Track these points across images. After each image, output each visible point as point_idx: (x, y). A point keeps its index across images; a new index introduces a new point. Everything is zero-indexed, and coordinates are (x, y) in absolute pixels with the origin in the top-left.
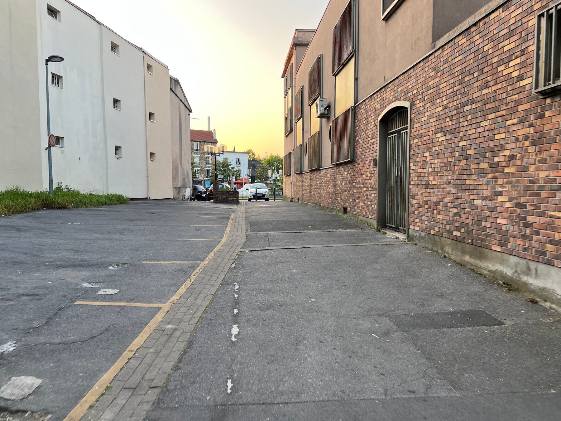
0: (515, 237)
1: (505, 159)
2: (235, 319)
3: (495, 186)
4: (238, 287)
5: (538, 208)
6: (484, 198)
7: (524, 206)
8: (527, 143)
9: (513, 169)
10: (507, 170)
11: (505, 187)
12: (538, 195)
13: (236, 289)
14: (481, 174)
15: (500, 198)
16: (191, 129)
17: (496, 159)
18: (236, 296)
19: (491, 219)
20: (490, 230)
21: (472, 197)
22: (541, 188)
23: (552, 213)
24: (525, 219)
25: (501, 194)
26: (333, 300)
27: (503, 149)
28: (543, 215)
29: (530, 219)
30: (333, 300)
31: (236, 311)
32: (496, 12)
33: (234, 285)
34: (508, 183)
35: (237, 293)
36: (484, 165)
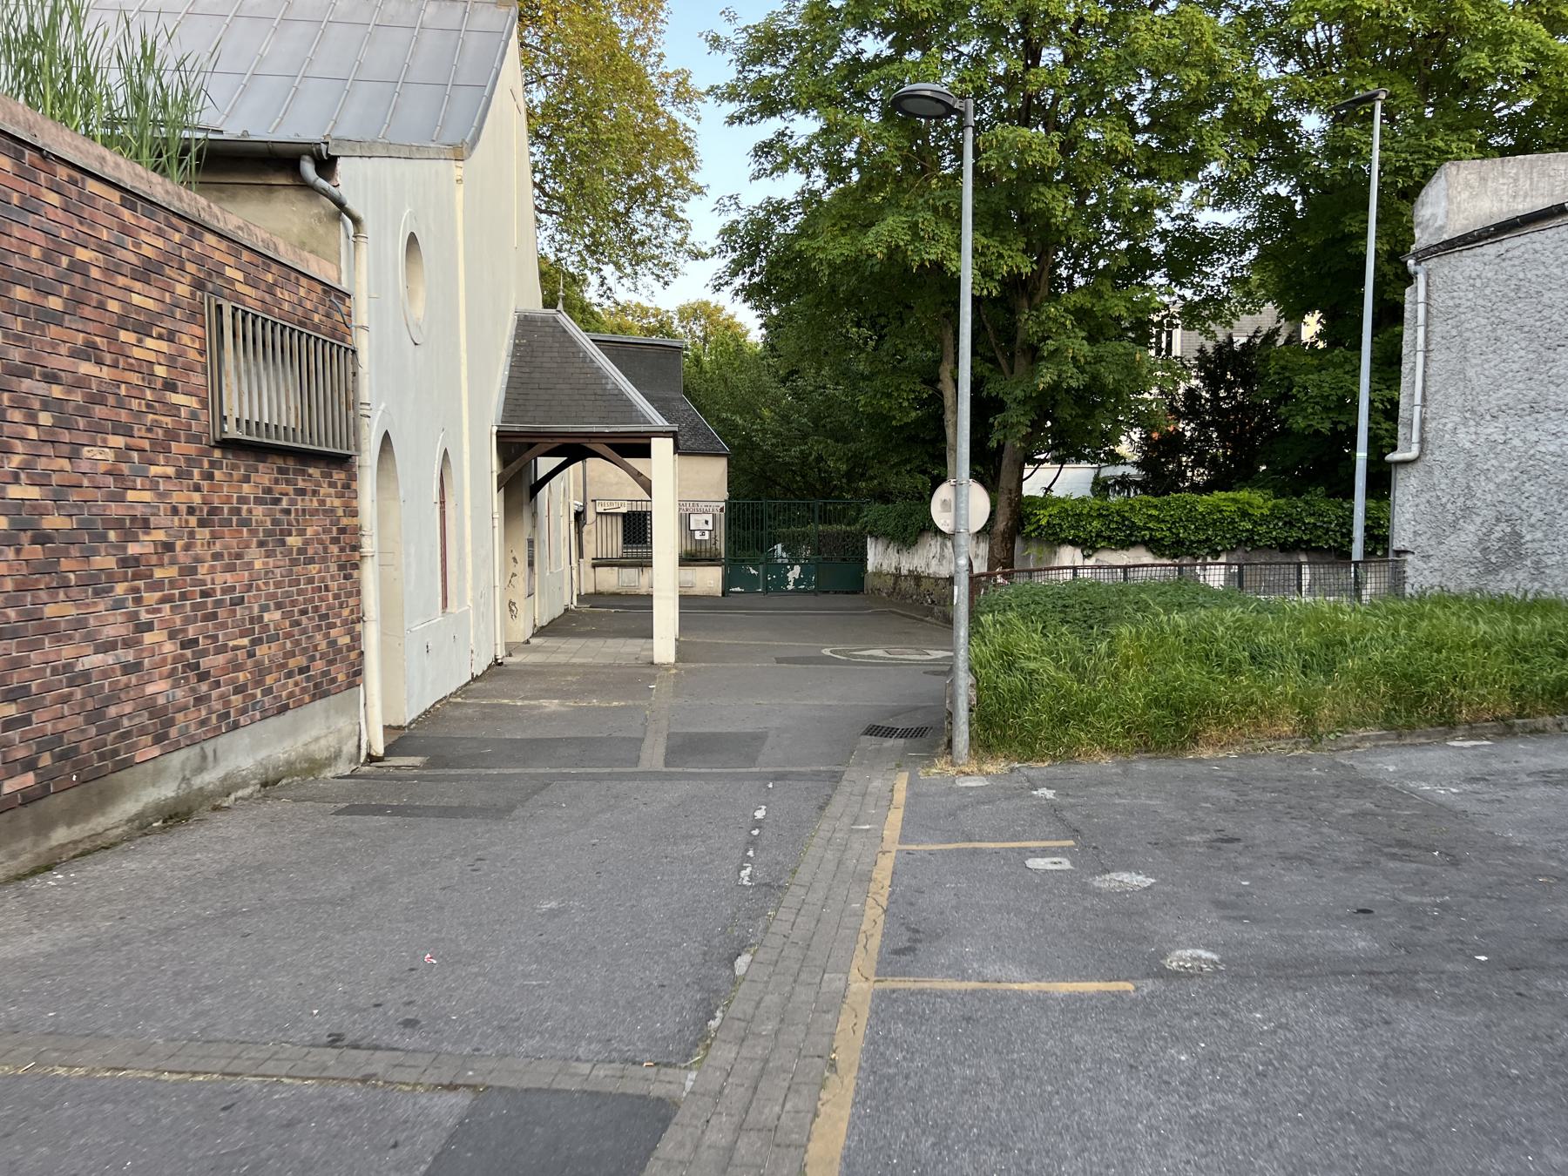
0: (185, 708)
1: (156, 548)
2: (758, 824)
3: (136, 613)
4: (743, 873)
5: (215, 638)
6: (108, 647)
7: (195, 642)
8: (193, 521)
9: (172, 572)
10: (158, 574)
11: (159, 611)
12: (214, 616)
13: (749, 870)
14: (97, 584)
15: (148, 638)
16: (672, 660)
17: (133, 549)
18: (751, 853)
19: (132, 693)
20: (130, 719)
21: (67, 652)
22: (219, 603)
23: (234, 643)
24: (197, 666)
25: (149, 627)
26: (1100, 192)
27: (146, 525)
28: (222, 649)
29: (205, 663)
30: (1100, 192)
31: (756, 832)
32: (112, 190)
33: (751, 877)
34: (163, 601)
35: (749, 859)
36: (105, 561)
